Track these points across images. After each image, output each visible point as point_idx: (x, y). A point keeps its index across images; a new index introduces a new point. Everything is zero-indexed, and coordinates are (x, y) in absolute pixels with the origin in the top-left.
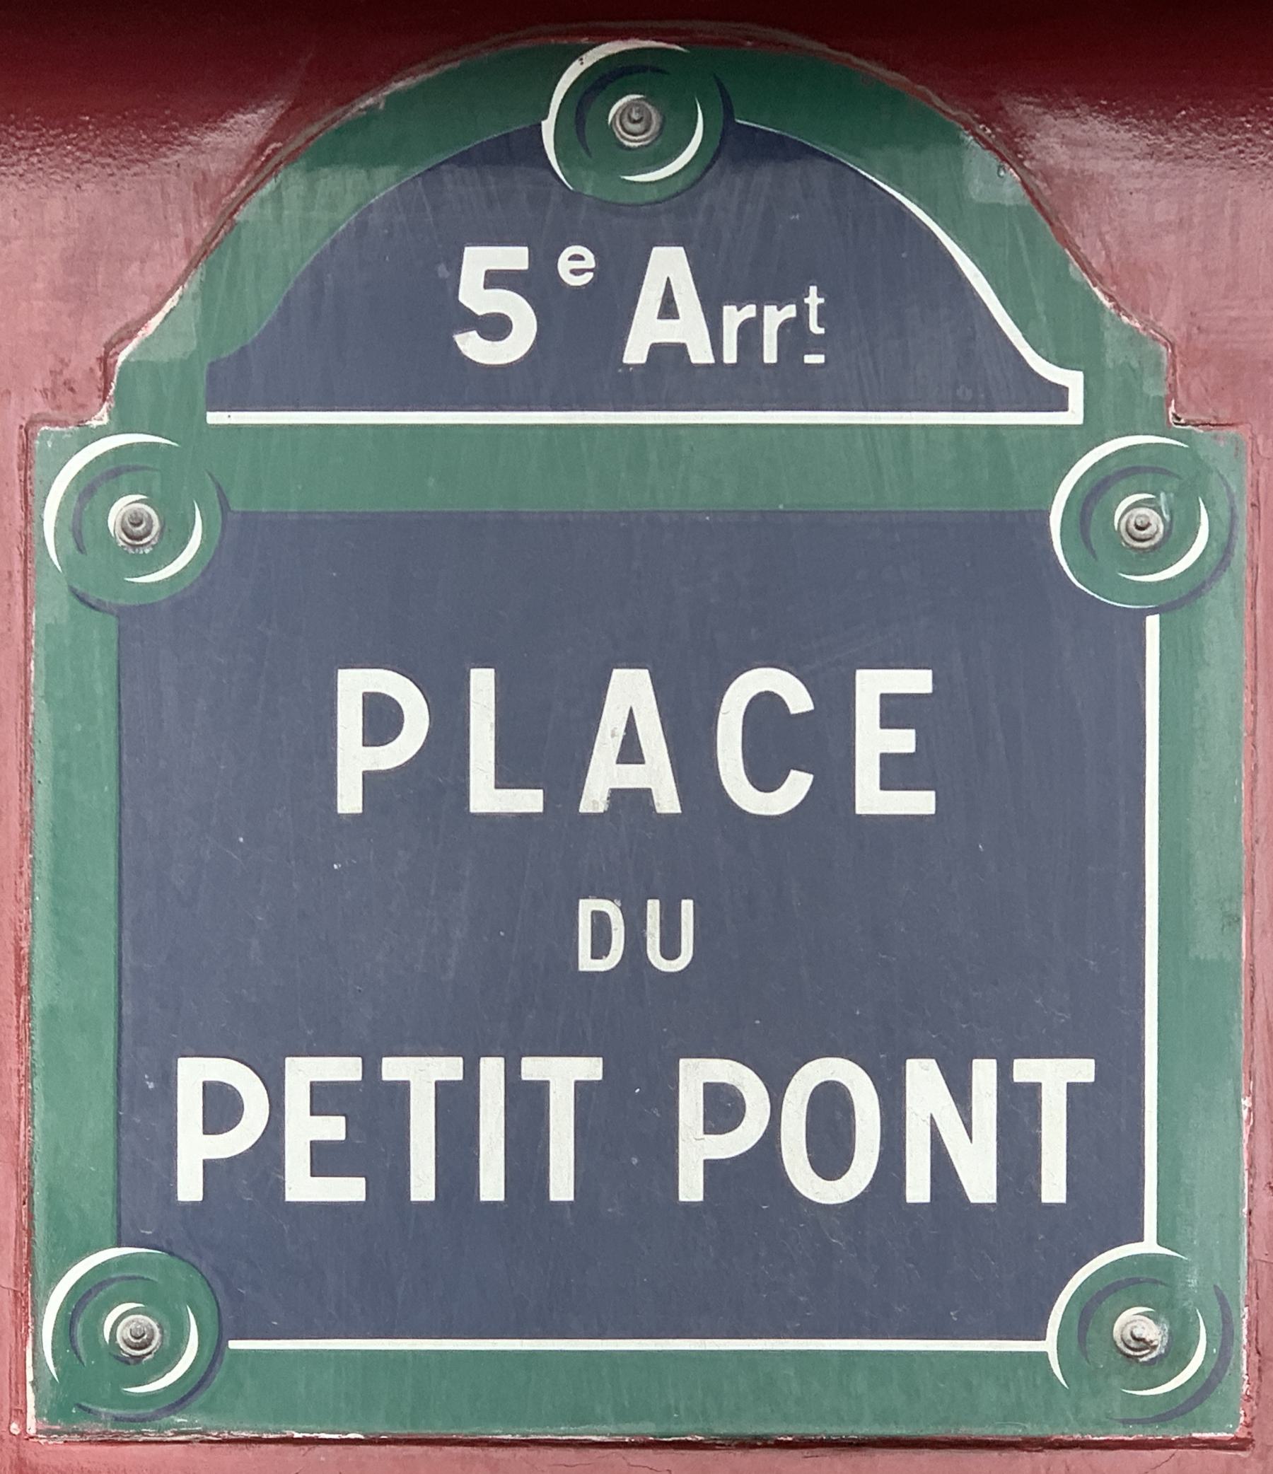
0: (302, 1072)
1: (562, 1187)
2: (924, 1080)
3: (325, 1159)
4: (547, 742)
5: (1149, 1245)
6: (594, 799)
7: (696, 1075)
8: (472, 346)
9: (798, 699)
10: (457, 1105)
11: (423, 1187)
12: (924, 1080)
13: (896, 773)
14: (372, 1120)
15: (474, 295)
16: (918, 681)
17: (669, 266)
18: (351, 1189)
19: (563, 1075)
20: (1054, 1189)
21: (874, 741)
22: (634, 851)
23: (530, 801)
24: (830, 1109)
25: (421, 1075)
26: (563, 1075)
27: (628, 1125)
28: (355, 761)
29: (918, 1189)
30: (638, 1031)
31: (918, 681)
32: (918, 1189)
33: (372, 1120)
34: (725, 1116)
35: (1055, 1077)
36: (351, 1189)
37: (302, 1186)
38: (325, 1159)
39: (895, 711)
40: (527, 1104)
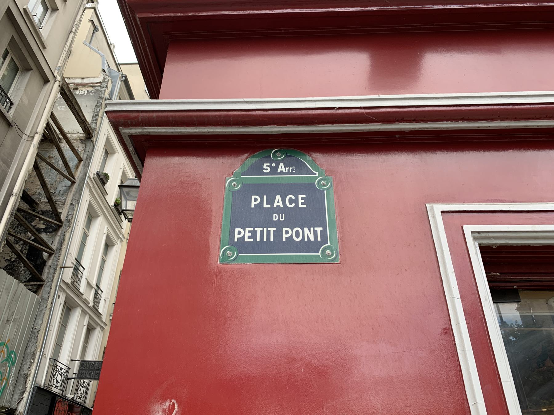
0: (247, 230)
1: (272, 239)
2: (306, 229)
3: (249, 237)
4: (271, 201)
5: (329, 244)
6: (275, 206)
7: (284, 229)
8: (264, 171)
9: (293, 198)
10: (262, 232)
11: (258, 240)
12: (306, 229)
13: (302, 203)
14: (254, 234)
15: (265, 167)
16: (304, 196)
17: (282, 165)
18: (251, 240)
19: (272, 230)
20: (319, 239)
21: (300, 201)
22: (279, 210)
23: (269, 206)
24: (297, 232)
25: (258, 230)
26: (272, 230)
27: (278, 234)
28: (253, 203)
29: (306, 239)
30: (279, 226)
31: (304, 196)
32: (306, 239)
33: (254, 234)
34: (287, 233)
35: (319, 229)
36: (251, 240)
37: (247, 240)
38: (249, 237)
39: (302, 198)
40: (268, 232)
